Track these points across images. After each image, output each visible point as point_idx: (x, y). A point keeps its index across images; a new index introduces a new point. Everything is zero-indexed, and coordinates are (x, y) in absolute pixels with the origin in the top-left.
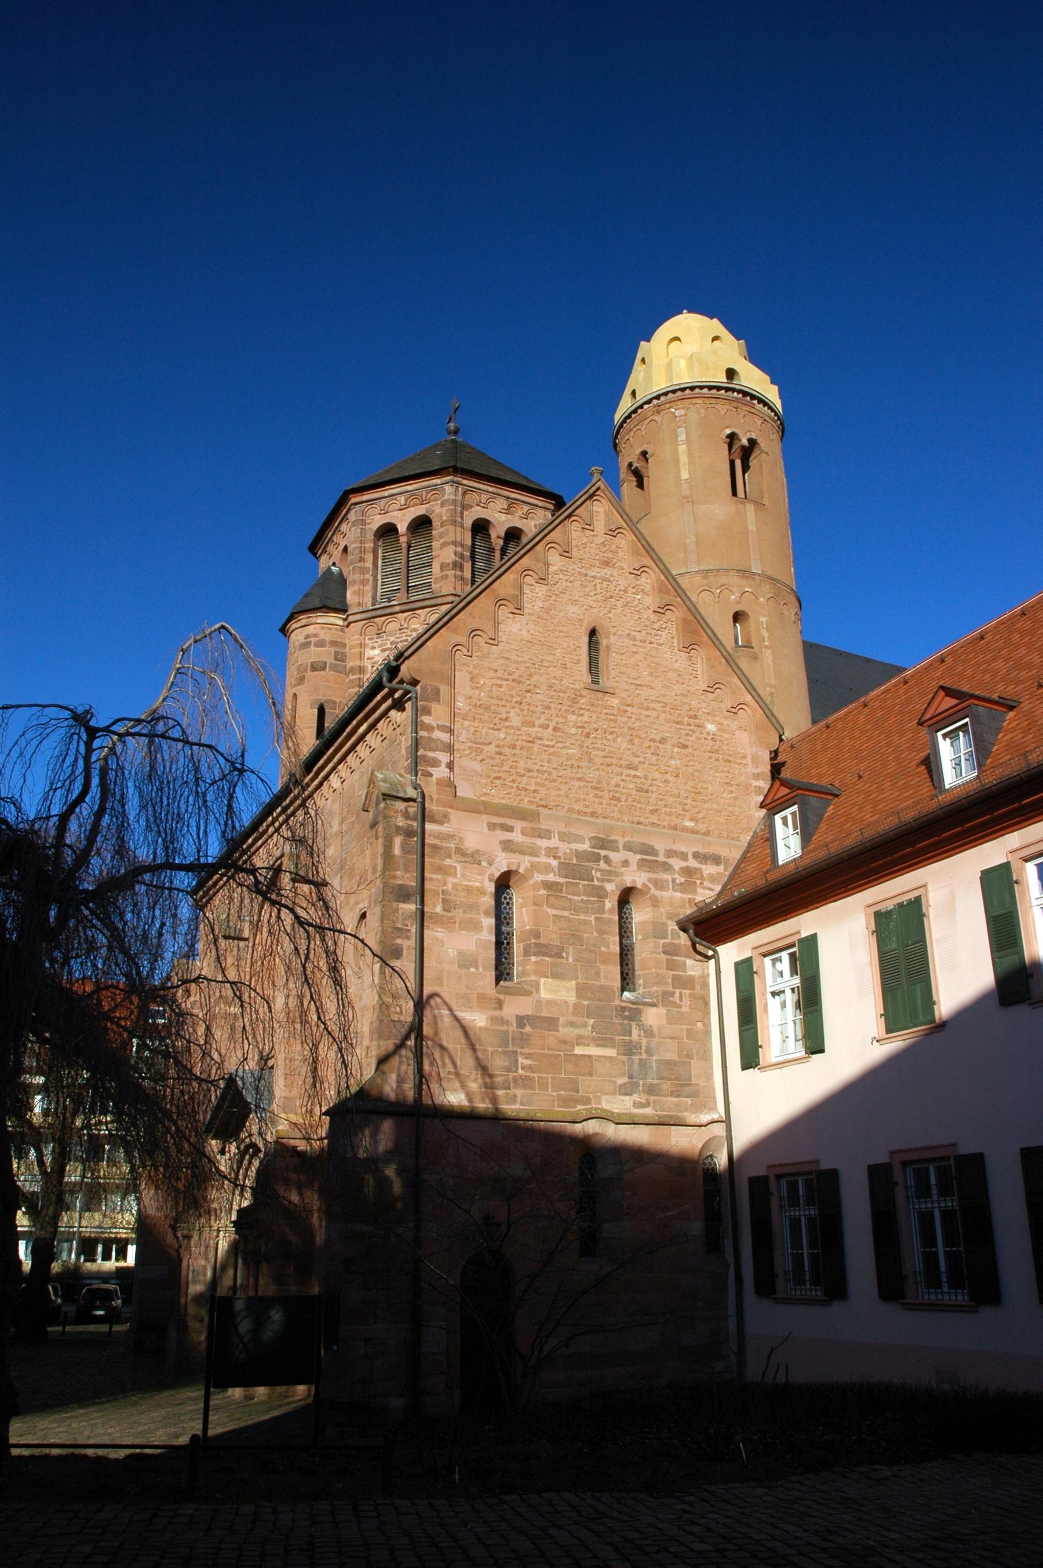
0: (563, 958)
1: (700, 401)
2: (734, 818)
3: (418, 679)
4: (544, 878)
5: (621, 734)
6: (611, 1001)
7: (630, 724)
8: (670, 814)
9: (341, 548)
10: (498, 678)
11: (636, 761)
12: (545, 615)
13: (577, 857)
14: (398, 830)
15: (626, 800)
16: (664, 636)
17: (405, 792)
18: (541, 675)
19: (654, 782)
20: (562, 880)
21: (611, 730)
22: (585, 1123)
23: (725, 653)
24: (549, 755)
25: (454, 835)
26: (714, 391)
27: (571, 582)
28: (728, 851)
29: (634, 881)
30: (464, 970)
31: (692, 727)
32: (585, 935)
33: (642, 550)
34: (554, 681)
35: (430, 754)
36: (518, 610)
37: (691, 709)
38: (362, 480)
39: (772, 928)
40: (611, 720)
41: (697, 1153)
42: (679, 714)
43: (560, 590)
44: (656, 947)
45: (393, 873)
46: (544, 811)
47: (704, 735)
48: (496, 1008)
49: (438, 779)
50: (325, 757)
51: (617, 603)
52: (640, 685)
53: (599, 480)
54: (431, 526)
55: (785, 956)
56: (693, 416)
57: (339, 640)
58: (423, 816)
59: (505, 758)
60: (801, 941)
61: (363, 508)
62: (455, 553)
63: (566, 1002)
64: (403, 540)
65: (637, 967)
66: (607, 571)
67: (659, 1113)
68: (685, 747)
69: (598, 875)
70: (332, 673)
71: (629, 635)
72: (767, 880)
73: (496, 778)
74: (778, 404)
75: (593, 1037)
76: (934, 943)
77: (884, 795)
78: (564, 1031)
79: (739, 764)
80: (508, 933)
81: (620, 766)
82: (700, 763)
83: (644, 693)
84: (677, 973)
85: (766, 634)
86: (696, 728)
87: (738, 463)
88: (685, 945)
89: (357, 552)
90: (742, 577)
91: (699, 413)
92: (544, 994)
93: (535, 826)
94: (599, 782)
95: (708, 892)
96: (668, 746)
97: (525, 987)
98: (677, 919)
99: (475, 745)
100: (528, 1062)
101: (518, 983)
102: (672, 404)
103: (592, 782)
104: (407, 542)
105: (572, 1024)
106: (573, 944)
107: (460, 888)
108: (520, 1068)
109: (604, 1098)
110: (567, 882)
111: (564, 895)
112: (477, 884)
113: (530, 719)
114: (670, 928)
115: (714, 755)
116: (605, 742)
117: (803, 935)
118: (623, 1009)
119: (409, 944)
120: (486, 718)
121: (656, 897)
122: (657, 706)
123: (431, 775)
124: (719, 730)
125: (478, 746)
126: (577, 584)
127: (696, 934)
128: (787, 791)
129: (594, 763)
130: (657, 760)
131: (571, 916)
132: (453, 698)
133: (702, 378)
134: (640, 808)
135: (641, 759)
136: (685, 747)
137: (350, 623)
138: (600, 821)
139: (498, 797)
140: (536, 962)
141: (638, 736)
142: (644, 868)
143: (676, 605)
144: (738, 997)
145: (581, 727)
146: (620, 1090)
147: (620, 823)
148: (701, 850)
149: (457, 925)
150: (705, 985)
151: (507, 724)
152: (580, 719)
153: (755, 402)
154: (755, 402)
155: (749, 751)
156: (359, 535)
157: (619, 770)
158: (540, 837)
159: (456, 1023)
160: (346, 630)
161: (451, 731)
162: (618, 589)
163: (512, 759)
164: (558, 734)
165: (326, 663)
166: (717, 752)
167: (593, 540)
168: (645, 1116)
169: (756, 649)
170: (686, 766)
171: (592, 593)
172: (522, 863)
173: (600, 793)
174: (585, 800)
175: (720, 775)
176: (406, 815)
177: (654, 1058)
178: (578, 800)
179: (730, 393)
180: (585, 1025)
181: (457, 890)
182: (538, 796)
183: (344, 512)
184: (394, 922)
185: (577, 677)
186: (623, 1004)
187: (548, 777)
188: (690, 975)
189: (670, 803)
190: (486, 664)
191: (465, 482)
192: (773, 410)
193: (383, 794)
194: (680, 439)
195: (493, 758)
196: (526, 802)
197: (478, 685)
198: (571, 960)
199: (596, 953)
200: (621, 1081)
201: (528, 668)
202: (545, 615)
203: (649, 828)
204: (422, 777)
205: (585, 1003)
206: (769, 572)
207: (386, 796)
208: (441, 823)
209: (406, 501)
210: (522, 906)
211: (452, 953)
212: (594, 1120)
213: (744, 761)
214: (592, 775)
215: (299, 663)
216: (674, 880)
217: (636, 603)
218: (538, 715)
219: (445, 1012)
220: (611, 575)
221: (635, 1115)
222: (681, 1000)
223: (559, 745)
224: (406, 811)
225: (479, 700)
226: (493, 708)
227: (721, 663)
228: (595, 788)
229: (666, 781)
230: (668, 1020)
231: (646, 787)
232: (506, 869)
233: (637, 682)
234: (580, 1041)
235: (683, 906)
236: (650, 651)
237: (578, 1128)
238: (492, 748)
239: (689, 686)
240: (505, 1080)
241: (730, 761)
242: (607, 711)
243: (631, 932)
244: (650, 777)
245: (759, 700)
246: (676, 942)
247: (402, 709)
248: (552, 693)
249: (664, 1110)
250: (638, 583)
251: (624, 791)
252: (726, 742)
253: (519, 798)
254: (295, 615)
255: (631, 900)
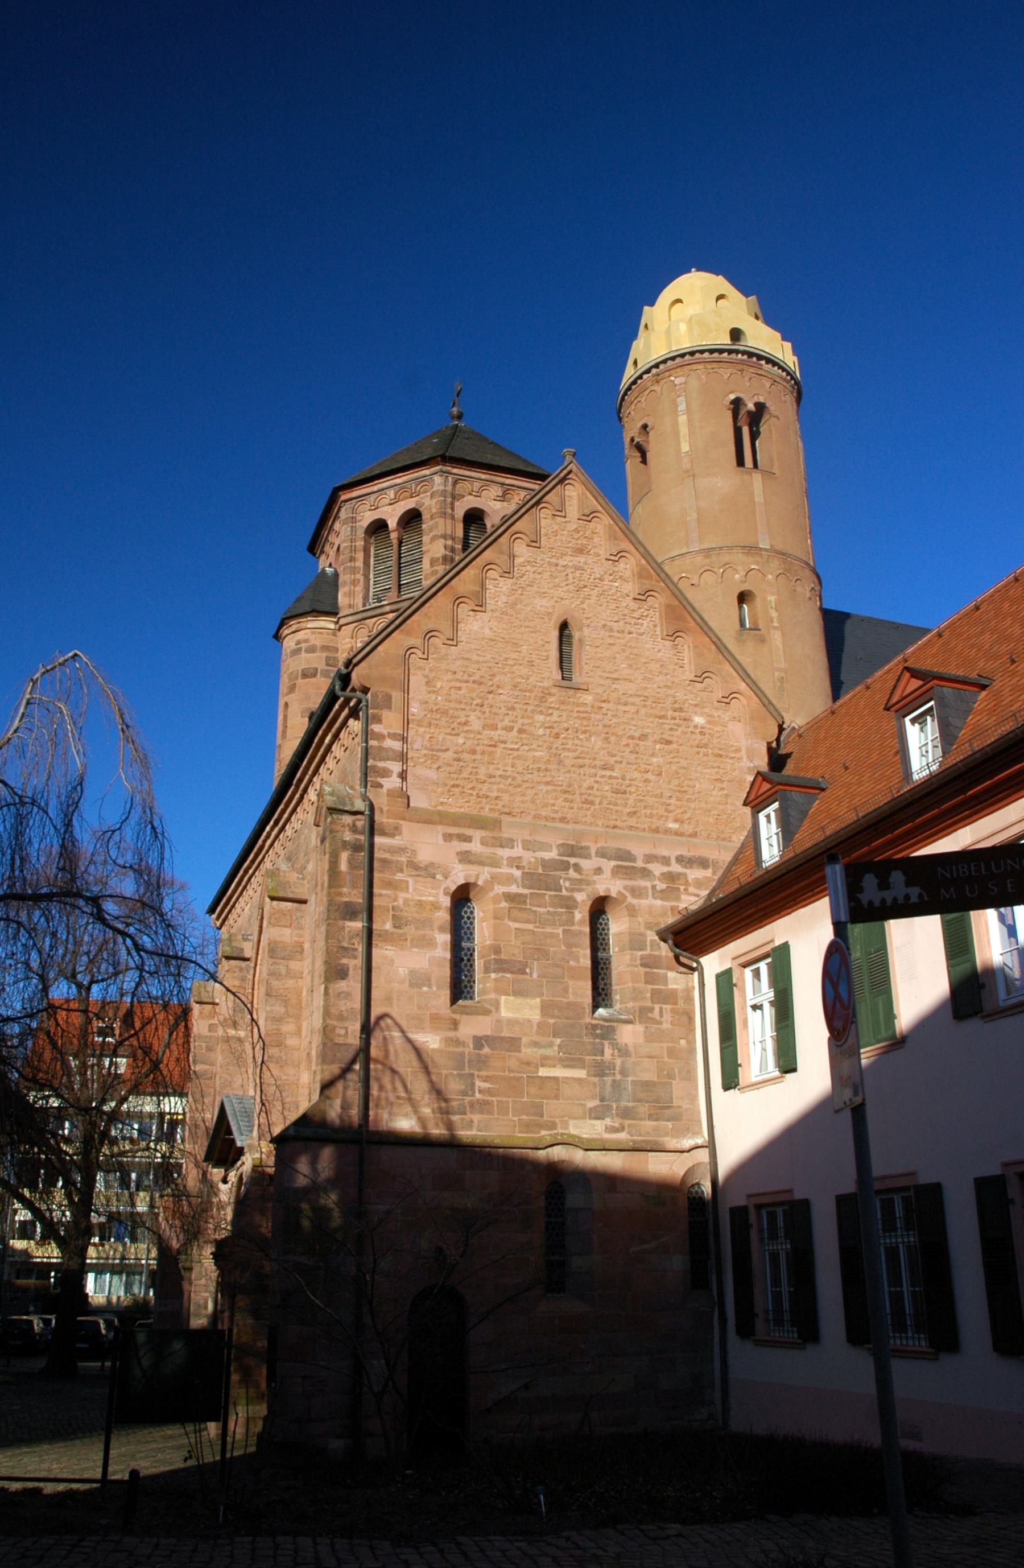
0: (527, 974)
1: (700, 366)
2: (725, 817)
3: (368, 686)
4: (506, 889)
5: (595, 733)
6: (580, 1018)
7: (606, 722)
8: (651, 816)
9: (335, 548)
10: (457, 680)
11: (613, 760)
12: (510, 611)
13: (543, 866)
14: (345, 845)
15: (600, 804)
16: (645, 624)
17: (352, 805)
18: (505, 674)
19: (632, 782)
20: (526, 891)
21: (583, 729)
22: (550, 1149)
23: (715, 639)
24: (513, 759)
25: (407, 848)
26: (716, 355)
27: (539, 573)
28: (717, 852)
29: (608, 890)
30: (416, 990)
31: (677, 721)
32: (552, 949)
33: (620, 534)
34: (519, 680)
35: (381, 764)
36: (480, 606)
37: (675, 702)
38: (353, 476)
39: (749, 936)
40: (584, 718)
41: (679, 1182)
42: (661, 708)
43: (527, 583)
44: (632, 960)
45: (338, 890)
46: (506, 819)
47: (691, 729)
48: (450, 1029)
49: (389, 790)
50: (301, 769)
51: (592, 592)
52: (617, 679)
53: (571, 462)
54: (421, 520)
55: (763, 966)
56: (694, 383)
57: (331, 645)
58: (372, 829)
59: (464, 764)
60: (776, 949)
61: (352, 505)
62: (445, 548)
63: (529, 1021)
64: (394, 536)
65: (614, 982)
66: (582, 559)
67: (635, 1138)
68: (669, 742)
69: (567, 884)
70: (323, 679)
71: (604, 626)
72: (740, 883)
73: (453, 786)
74: (790, 360)
75: (561, 1057)
76: (895, 951)
77: (862, 788)
78: (527, 1052)
79: (732, 758)
80: (469, 949)
81: (594, 767)
82: (686, 759)
83: (621, 687)
84: (656, 987)
85: (774, 614)
86: (681, 722)
87: (746, 431)
88: (667, 957)
89: (347, 551)
90: (747, 554)
91: (700, 379)
92: (505, 1013)
93: (496, 834)
94: (570, 785)
95: (693, 899)
96: (649, 743)
97: (486, 1006)
98: (657, 928)
99: (431, 753)
100: (487, 1085)
101: (478, 1002)
102: (672, 372)
103: (562, 786)
104: (398, 539)
105: (536, 1044)
106: (538, 959)
107: (411, 903)
108: (477, 1092)
109: (572, 1122)
110: (531, 894)
111: (528, 907)
112: (431, 899)
113: (492, 722)
114: (649, 939)
115: (702, 750)
116: (576, 742)
117: (777, 943)
118: (595, 1027)
119: (355, 964)
120: (443, 723)
121: (634, 906)
122: (636, 700)
123: (381, 786)
124: (709, 722)
125: (435, 753)
126: (546, 575)
127: (677, 945)
128: (769, 786)
129: (564, 766)
130: (636, 758)
131: (536, 930)
132: (406, 704)
133: (702, 342)
134: (617, 811)
135: (618, 758)
136: (669, 742)
137: (341, 626)
138: (570, 827)
139: (456, 805)
140: (496, 980)
141: (613, 734)
142: (619, 875)
143: (658, 590)
144: (719, 1011)
145: (550, 728)
146: (590, 1114)
147: (593, 828)
148: (685, 852)
149: (408, 943)
150: (690, 999)
151: (466, 728)
152: (548, 719)
153: (763, 362)
154: (763, 362)
155: (743, 743)
156: (349, 533)
157: (593, 771)
158: (502, 846)
159: (409, 1046)
160: (338, 633)
161: (404, 739)
162: (592, 577)
163: (472, 765)
164: (524, 736)
165: (317, 669)
166: (705, 746)
167: (565, 526)
168: (618, 1141)
169: (763, 632)
170: (671, 763)
171: (562, 584)
172: (481, 875)
173: (570, 797)
174: (553, 805)
175: (708, 771)
176: (354, 829)
177: (630, 1079)
178: (546, 805)
179: (733, 356)
180: (551, 1045)
181: (409, 905)
182: (501, 803)
183: (336, 511)
184: (339, 941)
185: (546, 675)
186: (594, 1022)
187: (512, 782)
188: (672, 989)
189: (651, 804)
190: (444, 666)
191: (455, 471)
192: (784, 370)
193: (329, 809)
194: (679, 409)
195: (450, 765)
196: (487, 810)
197: (435, 689)
198: (535, 976)
199: (563, 968)
200: (591, 1104)
201: (490, 668)
202: (510, 611)
203: (626, 832)
204: (372, 789)
205: (552, 1021)
206: (779, 547)
207: (332, 810)
208: (392, 836)
209: (396, 495)
210: (482, 921)
211: (402, 971)
212: (560, 1146)
213: (738, 755)
214: (562, 778)
215: (291, 670)
216: (654, 887)
217: (613, 591)
218: (501, 717)
219: (397, 1034)
220: (585, 563)
221: (607, 1141)
222: (661, 1016)
223: (525, 747)
224: (354, 825)
225: (436, 704)
226: (451, 712)
227: (710, 650)
228: (565, 792)
229: (646, 781)
230: (645, 1037)
231: (624, 787)
232: (463, 882)
233: (614, 676)
234: (545, 1062)
235: (664, 914)
236: (628, 641)
237: (542, 1154)
238: (449, 755)
239: (673, 676)
240: (461, 1105)
241: (721, 756)
242: (578, 709)
243: (607, 944)
244: (628, 777)
245: (754, 688)
246: (656, 953)
247: (357, 718)
248: (516, 693)
249: (640, 1135)
250: (616, 569)
251: (599, 793)
252: (716, 735)
253: (479, 806)
254: (286, 621)
255: (607, 909)
